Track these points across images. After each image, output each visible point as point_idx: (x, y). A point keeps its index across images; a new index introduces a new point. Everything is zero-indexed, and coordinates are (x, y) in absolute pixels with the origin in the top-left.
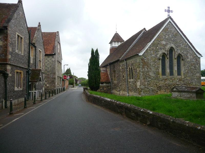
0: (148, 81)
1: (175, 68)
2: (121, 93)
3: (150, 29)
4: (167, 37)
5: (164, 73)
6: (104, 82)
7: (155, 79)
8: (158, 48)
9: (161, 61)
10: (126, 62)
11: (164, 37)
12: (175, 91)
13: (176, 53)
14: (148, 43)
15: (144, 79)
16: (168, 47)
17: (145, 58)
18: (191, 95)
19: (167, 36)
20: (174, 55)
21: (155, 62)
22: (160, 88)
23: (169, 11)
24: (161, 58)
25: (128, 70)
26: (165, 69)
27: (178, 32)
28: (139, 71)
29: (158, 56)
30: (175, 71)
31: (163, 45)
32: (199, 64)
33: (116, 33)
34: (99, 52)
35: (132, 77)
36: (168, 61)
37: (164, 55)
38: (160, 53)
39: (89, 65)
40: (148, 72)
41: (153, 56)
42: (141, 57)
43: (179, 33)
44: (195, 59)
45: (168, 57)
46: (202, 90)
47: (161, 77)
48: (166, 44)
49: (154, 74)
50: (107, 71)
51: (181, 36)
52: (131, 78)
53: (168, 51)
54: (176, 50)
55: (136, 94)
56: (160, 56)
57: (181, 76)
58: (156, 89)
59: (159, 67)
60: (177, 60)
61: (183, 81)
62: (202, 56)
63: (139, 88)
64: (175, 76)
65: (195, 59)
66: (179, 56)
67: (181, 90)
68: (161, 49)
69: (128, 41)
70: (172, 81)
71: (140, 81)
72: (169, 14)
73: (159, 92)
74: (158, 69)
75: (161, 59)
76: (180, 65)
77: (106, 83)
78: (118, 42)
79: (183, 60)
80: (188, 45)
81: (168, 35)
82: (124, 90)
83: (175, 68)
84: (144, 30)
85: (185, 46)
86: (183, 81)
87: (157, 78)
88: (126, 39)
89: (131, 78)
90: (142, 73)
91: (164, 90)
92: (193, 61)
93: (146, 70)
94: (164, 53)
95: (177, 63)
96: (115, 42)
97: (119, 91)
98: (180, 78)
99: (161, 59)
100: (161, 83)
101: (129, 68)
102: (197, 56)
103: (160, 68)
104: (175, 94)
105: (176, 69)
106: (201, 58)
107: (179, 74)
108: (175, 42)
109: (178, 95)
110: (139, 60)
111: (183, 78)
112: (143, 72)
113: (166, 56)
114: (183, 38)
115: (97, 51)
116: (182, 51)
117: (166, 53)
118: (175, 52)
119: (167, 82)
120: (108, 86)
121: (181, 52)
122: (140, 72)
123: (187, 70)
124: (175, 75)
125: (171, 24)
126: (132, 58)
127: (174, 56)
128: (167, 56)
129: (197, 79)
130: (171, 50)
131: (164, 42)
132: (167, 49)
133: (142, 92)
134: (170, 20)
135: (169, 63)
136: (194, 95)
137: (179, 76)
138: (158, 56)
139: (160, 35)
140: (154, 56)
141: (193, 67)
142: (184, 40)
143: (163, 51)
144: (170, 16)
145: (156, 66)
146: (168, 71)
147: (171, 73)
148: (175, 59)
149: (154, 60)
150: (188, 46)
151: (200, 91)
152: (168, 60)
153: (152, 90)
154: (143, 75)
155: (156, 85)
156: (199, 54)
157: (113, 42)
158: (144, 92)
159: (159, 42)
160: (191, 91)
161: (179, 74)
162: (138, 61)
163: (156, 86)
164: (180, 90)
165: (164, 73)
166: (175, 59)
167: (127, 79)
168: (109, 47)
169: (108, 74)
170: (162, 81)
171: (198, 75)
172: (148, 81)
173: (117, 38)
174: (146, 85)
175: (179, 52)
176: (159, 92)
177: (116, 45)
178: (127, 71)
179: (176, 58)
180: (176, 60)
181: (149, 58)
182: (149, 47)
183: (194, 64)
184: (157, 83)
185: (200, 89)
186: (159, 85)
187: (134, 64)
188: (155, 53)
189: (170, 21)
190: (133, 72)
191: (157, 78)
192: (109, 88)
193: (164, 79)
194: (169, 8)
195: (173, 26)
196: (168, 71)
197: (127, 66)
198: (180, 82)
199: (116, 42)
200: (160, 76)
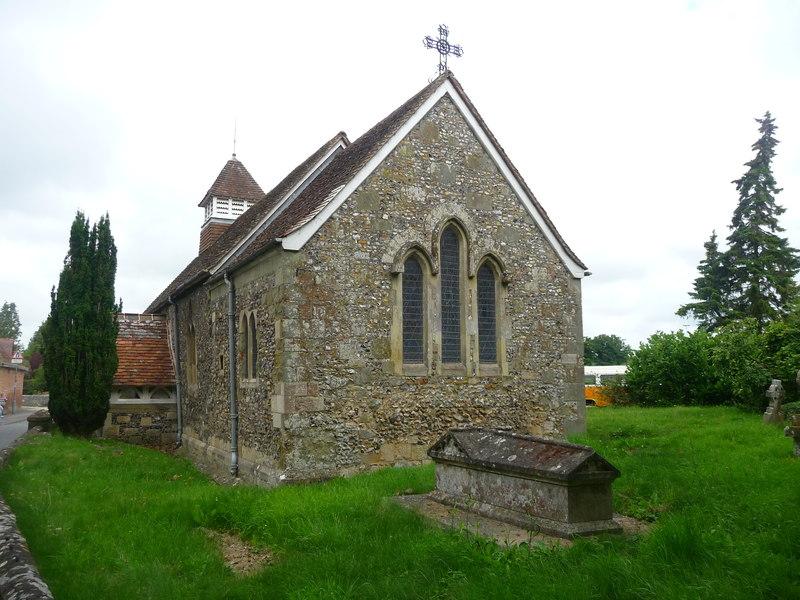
0: (331, 392)
1: (471, 326)
2: (211, 448)
3: (365, 135)
4: (432, 168)
5: (413, 347)
6: (140, 389)
7: (364, 377)
8: (385, 217)
9: (399, 287)
10: (233, 287)
11: (417, 166)
12: (449, 463)
13: (477, 251)
14: (337, 190)
15: (307, 377)
16: (437, 217)
17: (317, 263)
18: (541, 493)
19: (433, 165)
20: (466, 259)
21: (372, 291)
22: (391, 427)
23: (443, 47)
24: (400, 268)
25: (240, 326)
26: (420, 330)
27: (485, 150)
28: (283, 334)
29: (387, 258)
30: (468, 339)
31: (414, 203)
32: (575, 306)
33: (231, 158)
34: (114, 231)
35: (255, 370)
36: (433, 288)
37: (415, 258)
38: (398, 242)
39: (53, 295)
40: (330, 340)
41: (358, 254)
42: (298, 255)
43: (490, 157)
44: (560, 284)
45: (437, 265)
46: (607, 467)
47: (398, 369)
48: (428, 201)
49: (361, 353)
50: (164, 331)
51: (499, 170)
52: (250, 372)
53: (434, 239)
54: (474, 236)
55: (265, 458)
56: (396, 260)
57: (496, 362)
58: (372, 432)
59: (390, 317)
60: (479, 284)
61: (507, 389)
62: (587, 274)
63: (278, 430)
64: (468, 364)
65: (560, 284)
66: (489, 268)
67: (481, 455)
68: (402, 223)
69: (269, 195)
70: (454, 392)
71: (287, 389)
72: (443, 59)
73: (388, 451)
74: (382, 324)
75: (401, 275)
76: (494, 308)
77: (155, 390)
78: (239, 198)
79: (505, 284)
80: (529, 214)
81: (440, 160)
82: (223, 436)
83: (471, 326)
84: (341, 143)
85: (515, 221)
86: (507, 389)
87: (376, 374)
88: (267, 183)
89: (250, 372)
90: (297, 347)
91: (415, 439)
92: (552, 295)
93: (322, 329)
94: (417, 247)
95: (479, 301)
96: (222, 197)
97: (206, 436)
98: (493, 374)
99: (401, 275)
100: (400, 402)
101: (241, 319)
102: (568, 271)
103: (395, 319)
104: (454, 481)
105: (476, 331)
106: (585, 281)
107: (488, 353)
108: (474, 201)
109: (466, 490)
110: (285, 276)
111: (505, 373)
112: (302, 341)
113: (427, 259)
114: (505, 180)
115: (104, 226)
116: (503, 244)
117: (427, 246)
118: (468, 243)
119: (431, 395)
120: (162, 408)
121: (496, 246)
122: (287, 340)
123: (524, 334)
124: (469, 358)
125: (451, 106)
126: (252, 264)
127: (466, 265)
128: (430, 264)
129: (568, 380)
130: (453, 232)
131: (417, 193)
132: (431, 228)
133: (297, 453)
134: (447, 87)
135: (439, 296)
136: (560, 498)
137: (486, 366)
138: (387, 258)
139: (399, 154)
140: (364, 256)
141: (549, 323)
142: (514, 191)
143: (413, 235)
144: (450, 72)
145: (375, 312)
146: (434, 336)
147: (452, 350)
148: (471, 278)
149: (363, 277)
150: (527, 220)
151: (592, 470)
152: (436, 282)
153: (352, 438)
154: (305, 355)
155: (373, 408)
156: (573, 260)
157: (215, 200)
158: (304, 452)
159: (394, 186)
160: (537, 466)
161: (488, 353)
162: (278, 281)
163: (370, 415)
164: (476, 455)
165: (413, 347)
166: (471, 278)
167: (235, 373)
168: (199, 218)
169: (171, 345)
170: (402, 388)
171: (571, 358)
172: (331, 392)
173: (233, 181)
174: (315, 413)
175: (489, 245)
176: (388, 451)
177: (230, 211)
178: (235, 330)
179: (473, 272)
180: (474, 286)
181: (340, 265)
182: (341, 208)
183: (554, 307)
184: (378, 401)
185: (595, 460)
186: (390, 414)
187: (264, 297)
188: (373, 241)
189: (447, 96)
190: (259, 341)
191: (376, 374)
192: (169, 415)
193: (413, 381)
194: (443, 31)
195: (464, 119)
196: (434, 336)
197: (234, 308)
198: (491, 393)
199: (230, 202)
200: (392, 365)
